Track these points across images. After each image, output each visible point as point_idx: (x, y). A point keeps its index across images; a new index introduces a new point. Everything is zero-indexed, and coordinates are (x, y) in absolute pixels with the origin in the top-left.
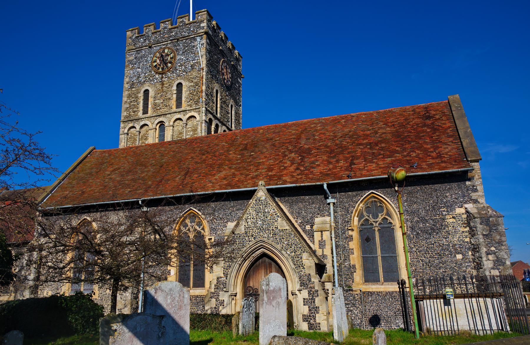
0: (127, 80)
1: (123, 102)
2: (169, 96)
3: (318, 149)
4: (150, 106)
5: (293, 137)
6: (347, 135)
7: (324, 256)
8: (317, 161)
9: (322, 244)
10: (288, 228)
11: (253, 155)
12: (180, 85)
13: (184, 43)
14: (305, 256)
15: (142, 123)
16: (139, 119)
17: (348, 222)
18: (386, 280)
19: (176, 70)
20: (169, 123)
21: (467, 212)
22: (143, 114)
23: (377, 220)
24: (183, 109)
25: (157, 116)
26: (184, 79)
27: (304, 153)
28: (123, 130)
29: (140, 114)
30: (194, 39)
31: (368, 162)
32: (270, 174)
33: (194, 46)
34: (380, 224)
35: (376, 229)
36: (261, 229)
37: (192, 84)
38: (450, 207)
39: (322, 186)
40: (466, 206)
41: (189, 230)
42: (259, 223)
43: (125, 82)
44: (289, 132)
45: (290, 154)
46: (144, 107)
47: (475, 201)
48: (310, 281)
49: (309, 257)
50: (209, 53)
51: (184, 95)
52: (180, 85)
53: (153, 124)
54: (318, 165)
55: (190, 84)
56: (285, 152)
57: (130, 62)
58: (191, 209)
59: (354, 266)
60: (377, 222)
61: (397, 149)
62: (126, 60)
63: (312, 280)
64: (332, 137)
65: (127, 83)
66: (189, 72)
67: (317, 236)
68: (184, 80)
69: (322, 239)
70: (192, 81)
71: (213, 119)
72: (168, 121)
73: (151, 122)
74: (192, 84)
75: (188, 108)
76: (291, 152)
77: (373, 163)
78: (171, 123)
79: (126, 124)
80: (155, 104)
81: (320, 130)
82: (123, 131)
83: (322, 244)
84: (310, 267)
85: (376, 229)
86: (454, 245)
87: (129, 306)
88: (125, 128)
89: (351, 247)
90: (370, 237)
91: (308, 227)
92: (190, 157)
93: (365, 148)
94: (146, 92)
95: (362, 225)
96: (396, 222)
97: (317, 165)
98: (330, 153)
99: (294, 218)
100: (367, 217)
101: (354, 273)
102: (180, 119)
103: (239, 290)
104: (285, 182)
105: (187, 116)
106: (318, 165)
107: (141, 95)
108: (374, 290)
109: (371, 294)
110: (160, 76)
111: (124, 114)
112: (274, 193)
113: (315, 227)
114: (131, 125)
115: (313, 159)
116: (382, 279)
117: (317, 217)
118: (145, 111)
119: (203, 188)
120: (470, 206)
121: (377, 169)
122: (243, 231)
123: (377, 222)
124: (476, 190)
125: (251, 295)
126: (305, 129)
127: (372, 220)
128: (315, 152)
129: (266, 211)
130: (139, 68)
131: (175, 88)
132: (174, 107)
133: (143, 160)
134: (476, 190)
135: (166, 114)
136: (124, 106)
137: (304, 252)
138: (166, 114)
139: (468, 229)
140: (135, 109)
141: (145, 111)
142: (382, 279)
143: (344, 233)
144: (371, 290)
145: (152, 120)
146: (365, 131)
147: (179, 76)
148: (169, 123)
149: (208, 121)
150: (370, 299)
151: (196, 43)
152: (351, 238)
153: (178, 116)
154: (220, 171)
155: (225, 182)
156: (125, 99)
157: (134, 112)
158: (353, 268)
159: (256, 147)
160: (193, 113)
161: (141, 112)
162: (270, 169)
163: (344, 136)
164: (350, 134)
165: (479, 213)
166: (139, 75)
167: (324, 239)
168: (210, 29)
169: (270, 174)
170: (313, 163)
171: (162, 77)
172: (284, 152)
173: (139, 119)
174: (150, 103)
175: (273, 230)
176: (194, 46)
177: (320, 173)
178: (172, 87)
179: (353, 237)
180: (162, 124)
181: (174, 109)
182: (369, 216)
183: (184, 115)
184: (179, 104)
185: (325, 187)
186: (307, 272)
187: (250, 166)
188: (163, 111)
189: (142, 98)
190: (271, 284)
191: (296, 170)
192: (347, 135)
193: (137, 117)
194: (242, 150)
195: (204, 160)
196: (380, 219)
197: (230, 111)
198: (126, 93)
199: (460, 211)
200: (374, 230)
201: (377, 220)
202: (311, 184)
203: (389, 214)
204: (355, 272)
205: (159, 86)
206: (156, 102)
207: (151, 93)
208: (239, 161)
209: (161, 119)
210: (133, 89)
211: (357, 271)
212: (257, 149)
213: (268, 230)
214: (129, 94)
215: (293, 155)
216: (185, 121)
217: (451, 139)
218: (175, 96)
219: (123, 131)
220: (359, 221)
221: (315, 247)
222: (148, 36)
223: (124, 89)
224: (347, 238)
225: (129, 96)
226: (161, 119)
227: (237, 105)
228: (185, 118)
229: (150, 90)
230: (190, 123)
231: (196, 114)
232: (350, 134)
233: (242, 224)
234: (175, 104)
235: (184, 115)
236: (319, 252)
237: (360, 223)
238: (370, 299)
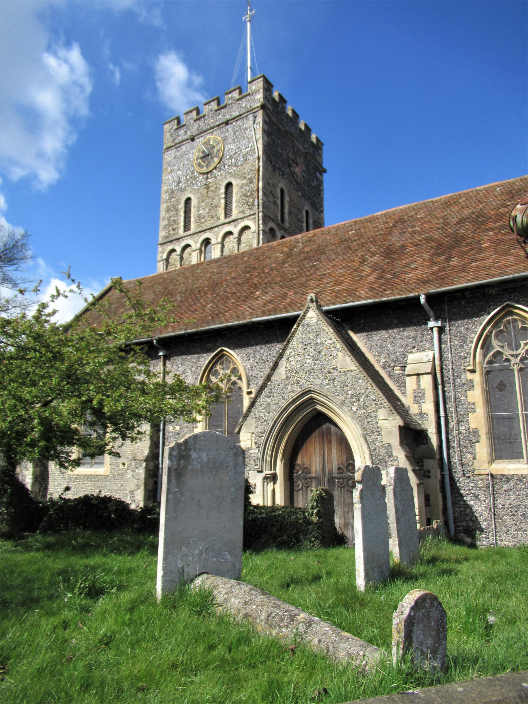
0: (164, 188)
1: (161, 218)
2: (215, 202)
3: (417, 245)
4: (192, 219)
5: (380, 233)
6: (467, 219)
7: (422, 415)
8: (414, 262)
9: (418, 397)
10: (353, 367)
11: (316, 265)
14: (382, 413)
15: (183, 244)
16: (179, 239)
17: (466, 358)
20: (217, 239)
22: (185, 231)
23: (518, 352)
24: (233, 217)
26: (235, 176)
27: (390, 253)
28: (161, 255)
29: (181, 232)
31: (501, 255)
32: (337, 288)
33: (246, 129)
34: (523, 359)
35: (516, 368)
37: (245, 181)
39: (418, 298)
42: (308, 361)
43: (163, 192)
44: (375, 227)
45: (371, 257)
46: (185, 221)
48: (390, 456)
49: (389, 415)
50: (268, 136)
51: (235, 198)
52: (229, 185)
53: (195, 243)
54: (416, 269)
55: (243, 182)
56: (365, 255)
57: (169, 164)
58: (222, 350)
59: (476, 432)
60: (517, 355)
62: (164, 162)
63: (394, 454)
64: (440, 226)
65: (166, 192)
66: (242, 165)
67: (410, 383)
68: (235, 178)
69: (419, 387)
70: (246, 178)
71: (276, 228)
72: (216, 237)
73: (194, 241)
74: (245, 181)
75: (241, 216)
76: (373, 254)
77: (510, 255)
78: (220, 240)
79: (165, 246)
80: (199, 217)
81: (422, 218)
82: (162, 257)
83: (418, 397)
84: (390, 432)
85: (516, 368)
87: (142, 488)
88: (163, 252)
89: (470, 400)
90: (505, 382)
91: (397, 371)
92: (230, 278)
93: (496, 234)
95: (490, 362)
96: (430, 200)
97: (413, 268)
98: (438, 249)
99: (375, 356)
100: (500, 349)
101: (477, 444)
102: (230, 233)
104: (359, 298)
105: (240, 227)
106: (416, 269)
107: (182, 206)
108: (513, 472)
109: (507, 478)
110: (205, 176)
111: (162, 234)
112: (345, 320)
113: (408, 371)
115: (407, 261)
117: (411, 352)
118: (187, 227)
119: (239, 318)
121: (516, 264)
122: (284, 377)
123: (517, 355)
126: (401, 221)
127: (507, 353)
128: (412, 251)
129: (319, 341)
130: (179, 170)
131: (223, 190)
132: (222, 216)
133: (171, 287)
135: (212, 228)
136: (163, 223)
137: (381, 408)
138: (212, 228)
140: (175, 226)
141: (187, 227)
143: (459, 377)
144: (506, 472)
146: (498, 209)
148: (217, 239)
149: (267, 230)
150: (505, 487)
152: (470, 385)
153: (227, 228)
154: (267, 293)
155: (271, 306)
156: (163, 214)
157: (174, 230)
158: (474, 436)
159: (323, 253)
161: (182, 228)
162: (338, 283)
163: (461, 222)
164: (473, 216)
166: (179, 179)
167: (422, 387)
168: (268, 101)
169: (337, 288)
170: (407, 265)
172: (363, 256)
173: (179, 239)
174: (192, 215)
175: (329, 372)
176: (246, 129)
177: (416, 282)
178: (220, 189)
179: (475, 383)
181: (222, 219)
182: (502, 347)
183: (235, 226)
185: (423, 299)
186: (386, 441)
187: (310, 280)
190: (194, 455)
191: (377, 279)
192: (467, 219)
193: (177, 237)
194: (301, 261)
195: (247, 279)
197: (305, 220)
198: (163, 206)
200: (512, 370)
201: (518, 352)
202: (399, 297)
204: (478, 442)
206: (200, 212)
208: (295, 276)
210: (173, 200)
211: (481, 440)
212: (323, 257)
213: (322, 372)
214: (168, 207)
215: (375, 258)
218: (223, 201)
219: (162, 257)
220: (485, 355)
221: (407, 400)
223: (162, 201)
224: (464, 384)
225: (168, 210)
227: (317, 211)
228: (236, 231)
232: (473, 216)
233: (282, 365)
235: (235, 226)
236: (414, 410)
237: (487, 359)
238: (505, 487)
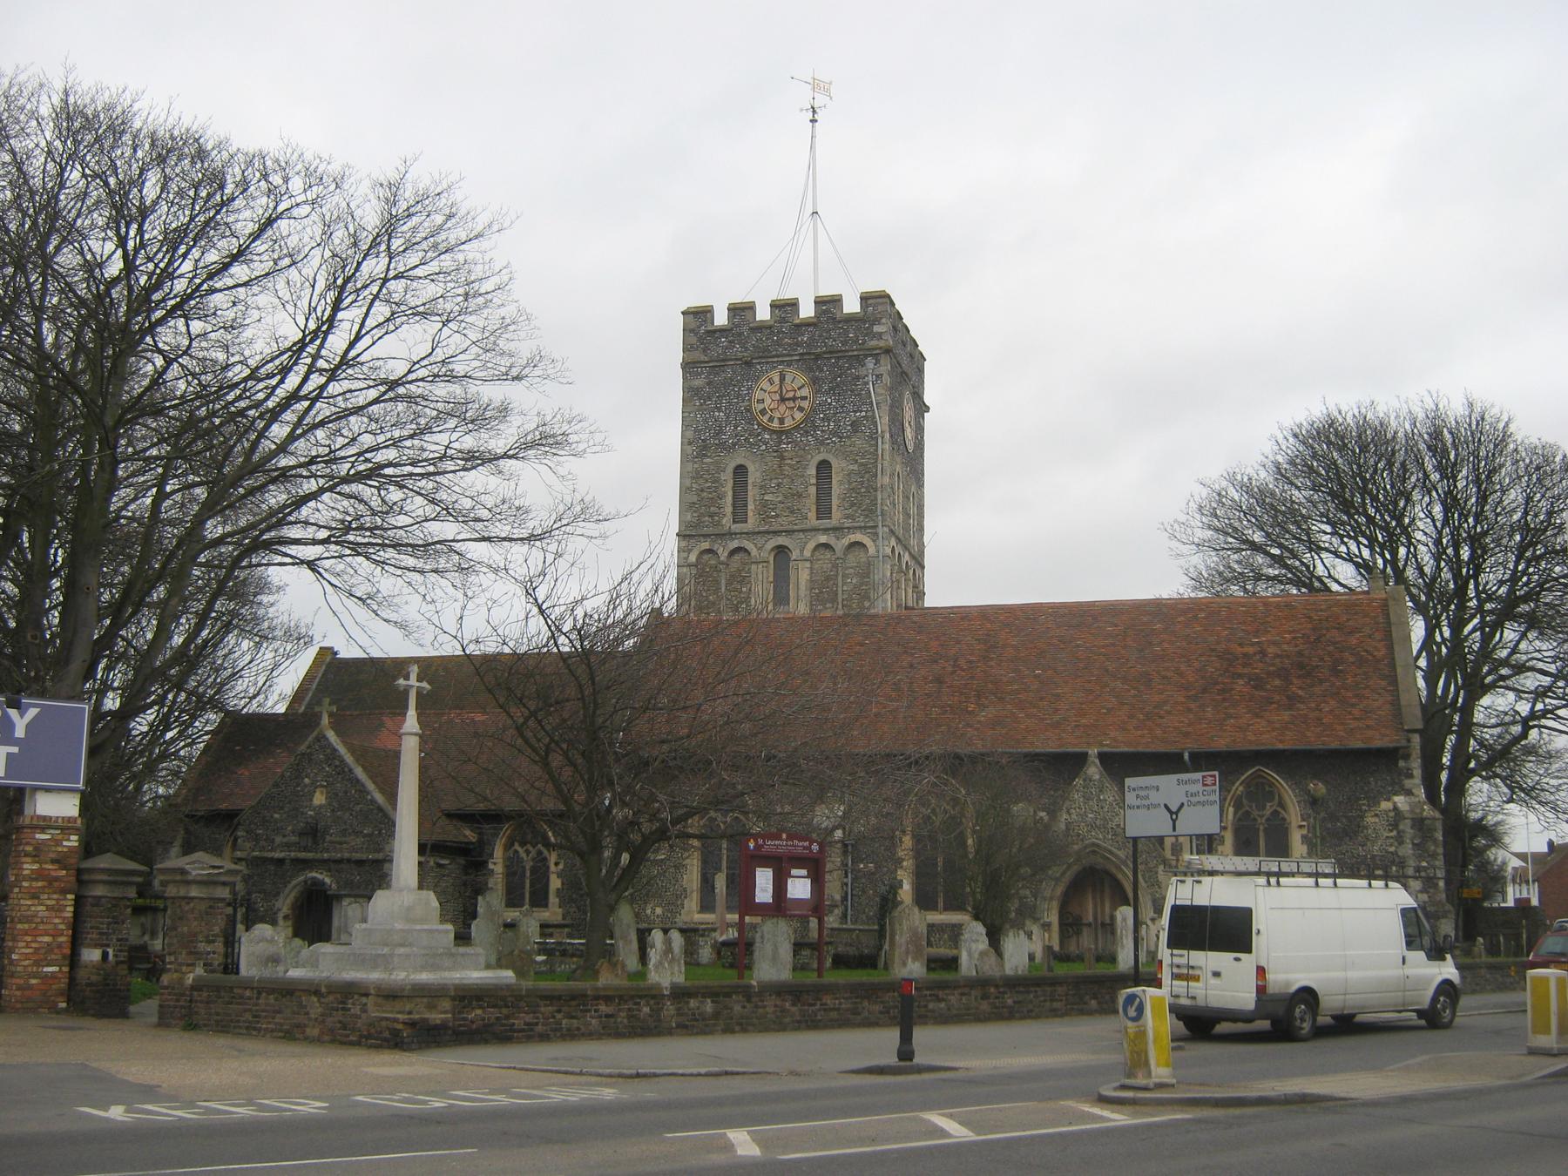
12: (824, 466)
13: (833, 366)
15: (735, 544)
18: (946, 909)
19: (815, 428)
20: (802, 551)
21: (1395, 808)
24: (834, 522)
25: (768, 532)
30: (859, 360)
33: (858, 378)
36: (1092, 826)
37: (855, 467)
38: (1374, 801)
40: (1396, 799)
41: (933, 811)
47: (1409, 793)
51: (837, 489)
52: (824, 466)
61: (1300, 692)
74: (855, 467)
78: (807, 554)
86: (1373, 857)
94: (740, 471)
103: (1054, 918)
105: (846, 541)
107: (727, 477)
114: (706, 545)
116: (941, 905)
118: (739, 515)
120: (1400, 800)
124: (1411, 776)
125: (1071, 925)
127: (1255, 813)
130: (719, 410)
132: (812, 515)
134: (1411, 776)
139: (1394, 833)
141: (739, 515)
142: (941, 905)
145: (760, 540)
147: (822, 443)
151: (862, 371)
153: (823, 539)
160: (858, 537)
161: (729, 516)
165: (1412, 811)
171: (780, 442)
176: (858, 378)
180: (781, 551)
181: (813, 520)
184: (824, 511)
188: (784, 522)
189: (730, 484)
196: (1268, 812)
199: (1385, 805)
203: (1282, 805)
205: (773, 462)
207: (754, 475)
209: (781, 540)
216: (839, 553)
217: (1384, 683)
218: (813, 490)
222: (741, 334)
226: (781, 540)
229: (751, 468)
230: (851, 558)
231: (866, 540)
234: (814, 508)
